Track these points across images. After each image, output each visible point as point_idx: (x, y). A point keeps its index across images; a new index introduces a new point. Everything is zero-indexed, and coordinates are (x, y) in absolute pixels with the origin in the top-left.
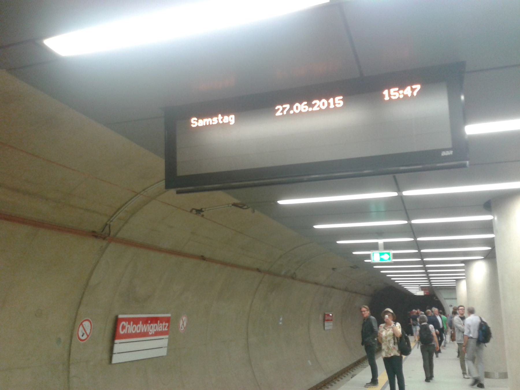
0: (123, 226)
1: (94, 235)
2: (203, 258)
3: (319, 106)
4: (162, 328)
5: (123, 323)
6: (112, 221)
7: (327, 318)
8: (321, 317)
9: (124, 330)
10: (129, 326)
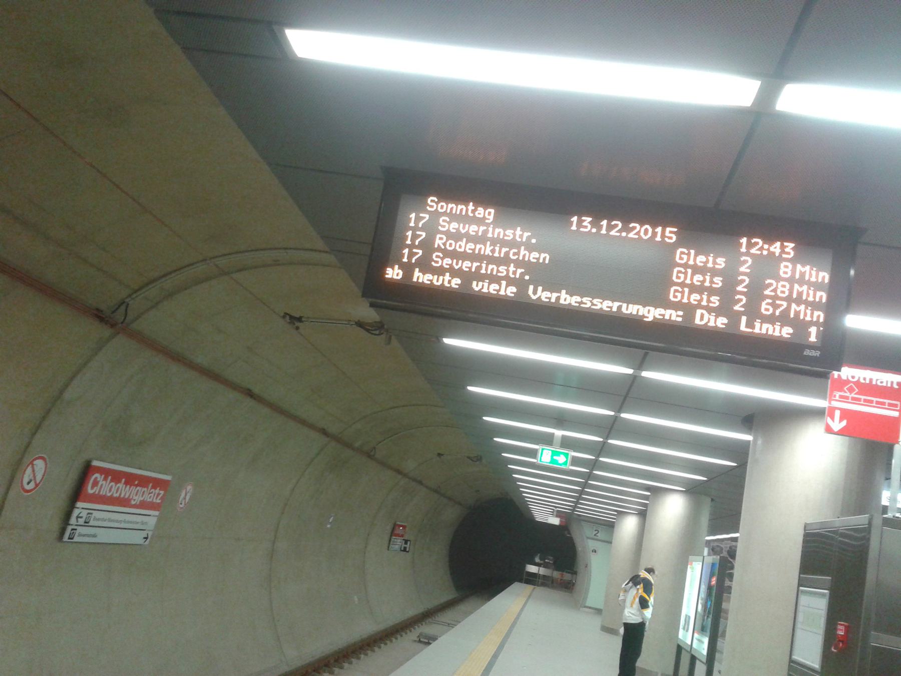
0: (148, 310)
1: (100, 316)
2: (250, 394)
3: (638, 233)
4: (152, 497)
5: (97, 475)
6: (133, 299)
7: (396, 532)
8: (389, 528)
9: (95, 488)
10: (104, 482)
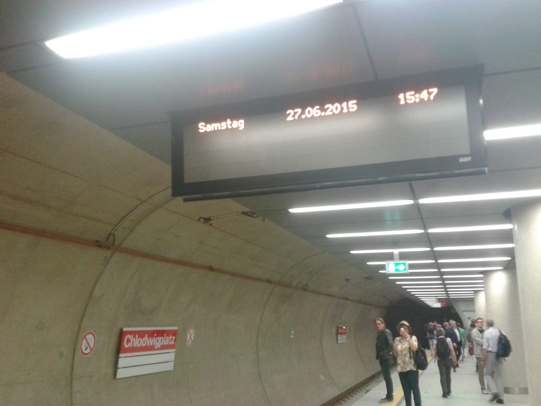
0: (128, 235)
1: (98, 244)
2: (211, 269)
3: (332, 111)
4: (168, 341)
5: (128, 336)
6: (116, 230)
7: (340, 331)
8: (334, 330)
9: (129, 344)
10: (134, 339)
